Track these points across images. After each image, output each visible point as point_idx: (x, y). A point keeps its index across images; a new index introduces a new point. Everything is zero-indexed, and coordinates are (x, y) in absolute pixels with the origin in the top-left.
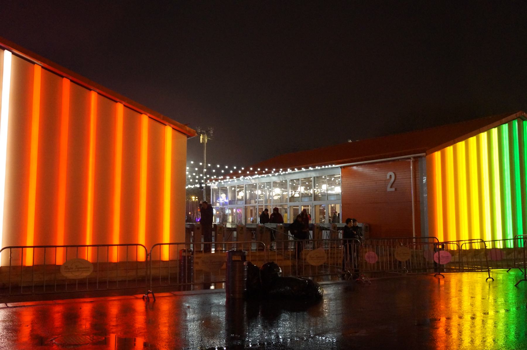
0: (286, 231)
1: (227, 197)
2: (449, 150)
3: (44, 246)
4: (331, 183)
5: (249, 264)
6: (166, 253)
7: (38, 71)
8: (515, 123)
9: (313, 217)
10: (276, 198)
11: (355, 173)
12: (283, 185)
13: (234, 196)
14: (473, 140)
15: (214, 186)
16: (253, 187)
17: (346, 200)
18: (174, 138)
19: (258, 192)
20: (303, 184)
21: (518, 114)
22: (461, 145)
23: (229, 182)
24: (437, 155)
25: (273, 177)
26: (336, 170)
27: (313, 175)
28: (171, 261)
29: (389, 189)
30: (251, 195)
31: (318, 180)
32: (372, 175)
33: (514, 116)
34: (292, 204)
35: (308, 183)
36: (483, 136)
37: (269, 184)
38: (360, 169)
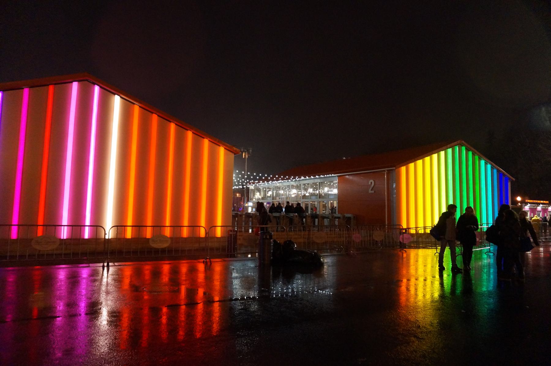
2: (412, 165)
3: (139, 226)
4: (330, 187)
7: (136, 109)
8: (457, 148)
10: (293, 196)
12: (298, 187)
15: (252, 187)
16: (278, 188)
17: (340, 197)
18: (225, 155)
19: (282, 192)
20: (312, 187)
21: (459, 142)
22: (420, 162)
23: (262, 185)
24: (403, 169)
27: (319, 181)
29: (370, 192)
31: (322, 185)
32: (360, 182)
33: (456, 143)
35: (315, 186)
37: (288, 186)
38: (351, 178)
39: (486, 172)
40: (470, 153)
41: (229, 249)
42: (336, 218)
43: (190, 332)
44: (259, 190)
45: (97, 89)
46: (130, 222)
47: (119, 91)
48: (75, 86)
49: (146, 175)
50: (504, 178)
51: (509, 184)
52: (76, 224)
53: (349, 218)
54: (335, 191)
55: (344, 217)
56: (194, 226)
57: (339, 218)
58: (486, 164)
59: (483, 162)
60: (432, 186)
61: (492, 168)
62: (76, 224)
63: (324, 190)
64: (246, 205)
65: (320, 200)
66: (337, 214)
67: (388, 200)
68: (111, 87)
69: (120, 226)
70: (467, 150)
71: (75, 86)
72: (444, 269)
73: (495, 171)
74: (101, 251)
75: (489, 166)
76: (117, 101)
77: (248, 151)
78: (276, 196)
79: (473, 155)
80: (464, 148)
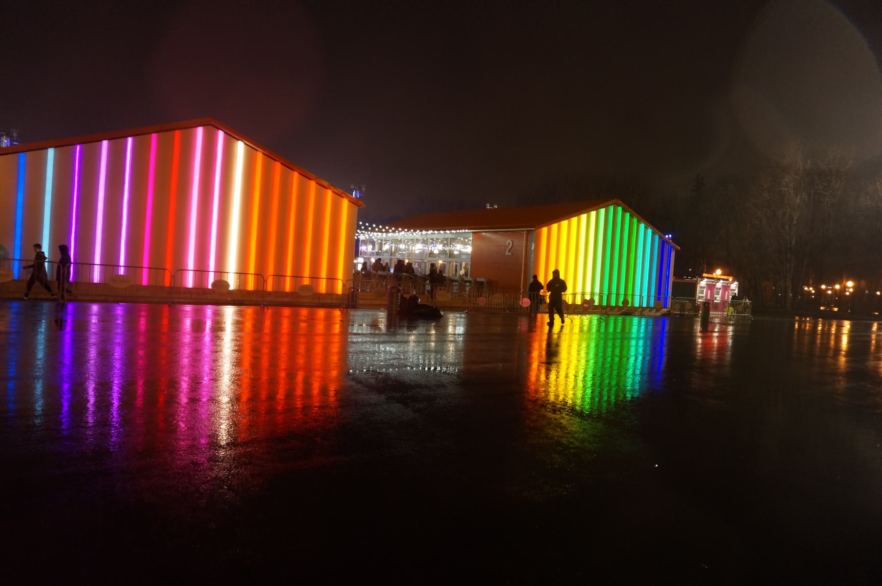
0: (425, 280)
1: (373, 249)
2: (555, 226)
3: (260, 276)
4: (465, 244)
5: (402, 296)
6: (339, 290)
7: (260, 156)
8: (611, 208)
9: (569, 290)
10: (417, 252)
11: (484, 238)
12: (425, 242)
13: (381, 248)
14: (574, 220)
15: (362, 237)
16: (397, 241)
17: (476, 259)
18: (349, 207)
19: (402, 246)
20: (442, 242)
21: (614, 201)
22: (565, 223)
23: (376, 236)
24: (545, 230)
25: (418, 234)
26: (468, 233)
27: (451, 236)
28: (343, 294)
29: (507, 253)
30: (396, 248)
31: (453, 240)
32: (498, 240)
33: (610, 202)
34: (431, 259)
35: (447, 242)
36: (584, 217)
37: (412, 240)
38: (488, 235)
39: (645, 240)
40: (628, 215)
41: (350, 302)
42: (466, 282)
43: (290, 395)
44: (373, 243)
45: (221, 134)
46: (252, 270)
47: (242, 137)
48: (200, 131)
49: (270, 225)
50: (666, 246)
51: (673, 254)
52: (201, 271)
53: (482, 283)
54: (469, 249)
55: (475, 281)
56: (315, 277)
57: (470, 282)
58: (646, 228)
59: (642, 226)
60: (582, 250)
61: (653, 234)
62: (201, 271)
63: (451, 247)
64: (355, 261)
65: (450, 259)
66: (469, 278)
67: (526, 265)
68: (235, 132)
69: (242, 274)
70: (624, 211)
71: (200, 131)
72: (548, 324)
73: (657, 237)
74: (220, 296)
75: (650, 231)
76: (240, 148)
77: (360, 189)
78: (395, 252)
79: (631, 217)
80: (620, 209)
